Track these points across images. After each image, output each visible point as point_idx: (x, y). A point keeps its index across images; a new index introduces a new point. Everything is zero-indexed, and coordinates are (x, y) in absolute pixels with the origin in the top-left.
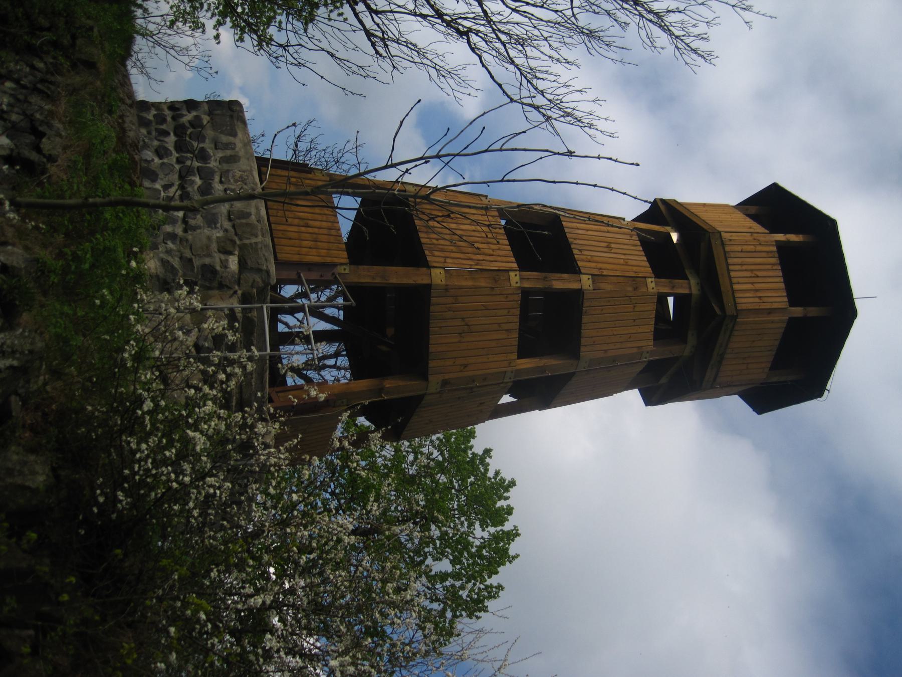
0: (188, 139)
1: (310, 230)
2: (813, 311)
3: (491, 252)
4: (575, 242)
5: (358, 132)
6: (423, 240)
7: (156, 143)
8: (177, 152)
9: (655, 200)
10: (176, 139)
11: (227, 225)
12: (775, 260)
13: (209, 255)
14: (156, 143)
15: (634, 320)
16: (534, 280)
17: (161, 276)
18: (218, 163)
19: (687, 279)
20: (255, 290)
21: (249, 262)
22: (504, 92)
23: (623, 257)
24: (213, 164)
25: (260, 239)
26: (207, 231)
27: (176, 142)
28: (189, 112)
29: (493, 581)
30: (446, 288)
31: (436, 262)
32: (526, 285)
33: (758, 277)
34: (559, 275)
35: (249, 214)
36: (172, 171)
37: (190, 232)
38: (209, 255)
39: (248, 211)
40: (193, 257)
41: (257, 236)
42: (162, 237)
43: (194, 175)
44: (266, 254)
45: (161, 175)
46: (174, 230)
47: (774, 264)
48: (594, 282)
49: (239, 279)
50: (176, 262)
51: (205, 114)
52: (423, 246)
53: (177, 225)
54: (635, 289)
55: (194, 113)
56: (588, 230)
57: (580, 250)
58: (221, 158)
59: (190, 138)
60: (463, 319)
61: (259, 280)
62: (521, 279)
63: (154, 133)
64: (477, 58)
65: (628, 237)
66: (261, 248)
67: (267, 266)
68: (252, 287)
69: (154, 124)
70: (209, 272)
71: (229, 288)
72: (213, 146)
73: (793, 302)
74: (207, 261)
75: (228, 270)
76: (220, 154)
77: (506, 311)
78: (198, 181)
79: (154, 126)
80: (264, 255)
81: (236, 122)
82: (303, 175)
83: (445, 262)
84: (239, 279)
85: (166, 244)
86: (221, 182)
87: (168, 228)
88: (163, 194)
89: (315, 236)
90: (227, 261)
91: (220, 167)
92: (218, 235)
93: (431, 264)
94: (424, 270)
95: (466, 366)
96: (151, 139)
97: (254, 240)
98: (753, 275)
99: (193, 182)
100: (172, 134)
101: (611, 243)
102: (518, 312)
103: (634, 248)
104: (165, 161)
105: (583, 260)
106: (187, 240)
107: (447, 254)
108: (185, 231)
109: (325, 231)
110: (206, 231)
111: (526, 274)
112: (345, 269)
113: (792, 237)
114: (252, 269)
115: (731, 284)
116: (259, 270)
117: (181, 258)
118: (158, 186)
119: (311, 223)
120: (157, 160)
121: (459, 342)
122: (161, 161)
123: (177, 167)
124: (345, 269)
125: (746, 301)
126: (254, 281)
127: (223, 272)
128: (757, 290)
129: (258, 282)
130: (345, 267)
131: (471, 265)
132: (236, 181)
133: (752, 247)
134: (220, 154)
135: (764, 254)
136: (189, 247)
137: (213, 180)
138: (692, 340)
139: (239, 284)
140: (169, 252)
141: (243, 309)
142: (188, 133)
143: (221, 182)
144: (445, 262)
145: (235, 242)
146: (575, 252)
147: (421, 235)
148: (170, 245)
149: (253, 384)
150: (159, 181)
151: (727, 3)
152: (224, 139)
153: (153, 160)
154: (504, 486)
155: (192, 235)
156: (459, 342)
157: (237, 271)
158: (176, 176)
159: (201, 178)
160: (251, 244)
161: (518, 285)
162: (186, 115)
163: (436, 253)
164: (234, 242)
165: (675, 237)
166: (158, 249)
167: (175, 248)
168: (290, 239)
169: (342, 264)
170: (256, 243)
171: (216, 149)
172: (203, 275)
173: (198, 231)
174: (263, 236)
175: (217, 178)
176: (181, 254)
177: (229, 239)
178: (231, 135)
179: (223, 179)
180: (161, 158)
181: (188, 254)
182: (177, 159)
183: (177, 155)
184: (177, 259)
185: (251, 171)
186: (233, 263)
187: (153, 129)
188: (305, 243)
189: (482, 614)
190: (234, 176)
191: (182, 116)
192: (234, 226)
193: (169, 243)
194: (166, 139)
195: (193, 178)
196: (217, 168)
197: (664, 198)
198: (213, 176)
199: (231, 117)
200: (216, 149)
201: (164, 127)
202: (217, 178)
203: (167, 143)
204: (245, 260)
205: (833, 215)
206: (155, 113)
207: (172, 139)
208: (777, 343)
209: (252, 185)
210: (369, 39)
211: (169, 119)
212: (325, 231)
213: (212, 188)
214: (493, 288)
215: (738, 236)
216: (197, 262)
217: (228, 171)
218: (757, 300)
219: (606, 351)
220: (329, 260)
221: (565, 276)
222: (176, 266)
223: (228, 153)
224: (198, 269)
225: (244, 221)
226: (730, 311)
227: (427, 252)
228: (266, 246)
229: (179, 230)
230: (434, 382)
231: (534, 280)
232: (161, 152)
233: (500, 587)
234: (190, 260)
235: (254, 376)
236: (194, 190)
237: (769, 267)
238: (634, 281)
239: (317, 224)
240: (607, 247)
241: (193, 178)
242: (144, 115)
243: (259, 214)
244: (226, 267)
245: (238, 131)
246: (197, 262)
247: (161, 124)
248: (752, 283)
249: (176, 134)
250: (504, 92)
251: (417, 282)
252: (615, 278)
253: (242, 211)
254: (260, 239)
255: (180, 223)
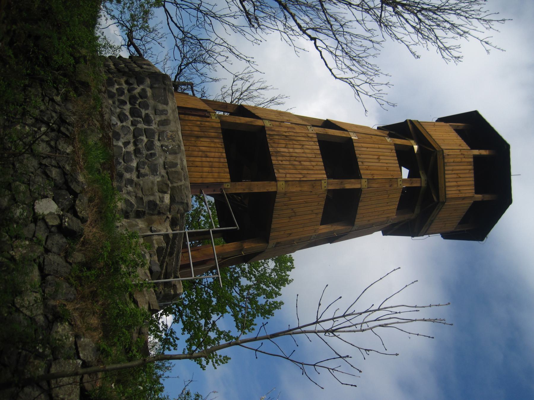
0: (137, 107)
1: (208, 159)
2: (488, 197)
3: (311, 167)
4: (360, 156)
5: (298, 295)
6: (274, 162)
7: (118, 110)
8: (132, 117)
9: (406, 121)
10: (131, 106)
11: (163, 172)
12: (471, 167)
13: (153, 194)
14: (118, 110)
15: (387, 203)
16: (335, 184)
17: (124, 209)
18: (157, 126)
19: (420, 177)
20: (179, 215)
21: (176, 199)
22: (332, 73)
23: (386, 165)
24: (154, 126)
25: (183, 182)
26: (151, 178)
27: (131, 108)
28: (139, 86)
29: (278, 299)
30: (285, 194)
31: (280, 177)
32: (331, 187)
33: (460, 177)
34: (349, 180)
35: (176, 164)
36: (129, 132)
37: (141, 178)
38: (153, 194)
39: (176, 162)
40: (143, 196)
41: (181, 181)
42: (124, 182)
43: (143, 135)
44: (187, 193)
45: (122, 136)
46: (131, 177)
47: (470, 170)
48: (368, 183)
49: (170, 208)
50: (133, 200)
51: (148, 87)
52: (274, 166)
53: (133, 173)
54: (391, 186)
55: (142, 87)
56: (367, 148)
57: (362, 162)
58: (159, 121)
59: (139, 106)
60: (292, 209)
61: (182, 209)
62: (328, 184)
63: (117, 103)
64: (319, 53)
65: (390, 151)
66: (184, 189)
67: (187, 201)
68: (177, 213)
69: (116, 96)
70: (153, 205)
71: (164, 214)
72: (153, 112)
73: (477, 192)
74: (151, 198)
75: (164, 203)
76: (158, 119)
77: (317, 203)
78: (145, 139)
79: (117, 97)
80: (185, 193)
81: (167, 92)
82: (205, 119)
83: (286, 177)
84: (170, 208)
85: (127, 187)
86: (159, 140)
87: (127, 176)
88: (124, 150)
89: (211, 164)
90: (163, 197)
91: (158, 128)
92: (158, 180)
93: (277, 179)
94: (273, 183)
95: (290, 234)
96: (115, 108)
97: (180, 183)
98: (458, 177)
99: (142, 140)
100: (128, 103)
101: (380, 156)
102: (323, 203)
103: (392, 158)
104: (124, 124)
105: (363, 169)
106: (140, 185)
107: (287, 171)
108: (138, 177)
109: (217, 160)
110: (151, 177)
111: (331, 180)
112: (228, 186)
113: (484, 152)
114: (178, 202)
115: (445, 182)
116: (182, 203)
117: (136, 197)
118: (120, 144)
119: (208, 154)
120: (119, 124)
121: (289, 222)
122: (122, 124)
123: (132, 128)
124: (228, 186)
125: (451, 192)
126: (179, 209)
127: (161, 205)
128: (458, 186)
129: (181, 210)
130: (228, 184)
131: (300, 178)
132: (168, 139)
133: (459, 159)
134: (158, 119)
135: (466, 164)
136: (140, 189)
137: (154, 138)
138: (417, 211)
139: (170, 211)
140: (128, 193)
141: (173, 234)
142: (138, 102)
143: (159, 140)
144: (286, 177)
145: (168, 185)
146: (360, 163)
147: (273, 158)
148: (130, 188)
149: (174, 264)
150: (121, 139)
151: (477, 38)
152: (161, 107)
153: (117, 124)
154: (293, 260)
155: (142, 180)
156: (289, 222)
157: (169, 204)
158: (132, 136)
159: (146, 137)
160: (178, 186)
161: (326, 188)
162: (136, 88)
163: (281, 171)
164: (167, 185)
165: (416, 147)
166: (122, 191)
167: (132, 190)
168: (197, 167)
169: (226, 183)
170: (181, 186)
171: (156, 114)
172: (149, 207)
173: (146, 177)
174: (185, 180)
175: (156, 137)
176: (136, 194)
177: (165, 183)
178: (165, 104)
179: (160, 138)
180: (122, 122)
181: (140, 194)
182: (132, 122)
183: (131, 119)
184: (134, 198)
185: (177, 131)
186: (167, 199)
187: (116, 99)
188: (206, 169)
189: (270, 316)
190: (167, 136)
191: (134, 89)
192: (167, 173)
193: (129, 186)
194: (125, 107)
195: (142, 138)
196: (157, 129)
197: (412, 119)
198: (154, 136)
199: (165, 89)
200: (156, 114)
201: (122, 98)
202: (156, 137)
203: (125, 110)
204: (174, 197)
205: (508, 141)
206: (118, 87)
207: (128, 106)
208: (464, 214)
209: (178, 142)
210: (248, 17)
211: (126, 91)
212: (217, 160)
213: (154, 145)
214: (311, 191)
215: (452, 152)
216: (146, 199)
217: (163, 132)
218: (458, 192)
219: (369, 220)
220: (219, 180)
221: (353, 180)
222: (133, 202)
223: (163, 117)
224: (146, 203)
225: (173, 169)
226: (441, 200)
227: (275, 171)
228: (187, 187)
229: (134, 176)
230: (272, 243)
231: (335, 184)
232: (122, 117)
233: (282, 303)
234: (142, 199)
235: (174, 260)
236: (143, 147)
237: (467, 171)
238: (391, 181)
239: (213, 154)
240: (378, 159)
241: (142, 138)
242: (110, 89)
243: (183, 164)
244: (163, 202)
245: (169, 100)
246: (146, 199)
247: (122, 96)
248: (456, 182)
249: (130, 103)
250: (332, 73)
251: (269, 191)
252: (380, 180)
253: (172, 162)
254: (183, 182)
255: (134, 171)
